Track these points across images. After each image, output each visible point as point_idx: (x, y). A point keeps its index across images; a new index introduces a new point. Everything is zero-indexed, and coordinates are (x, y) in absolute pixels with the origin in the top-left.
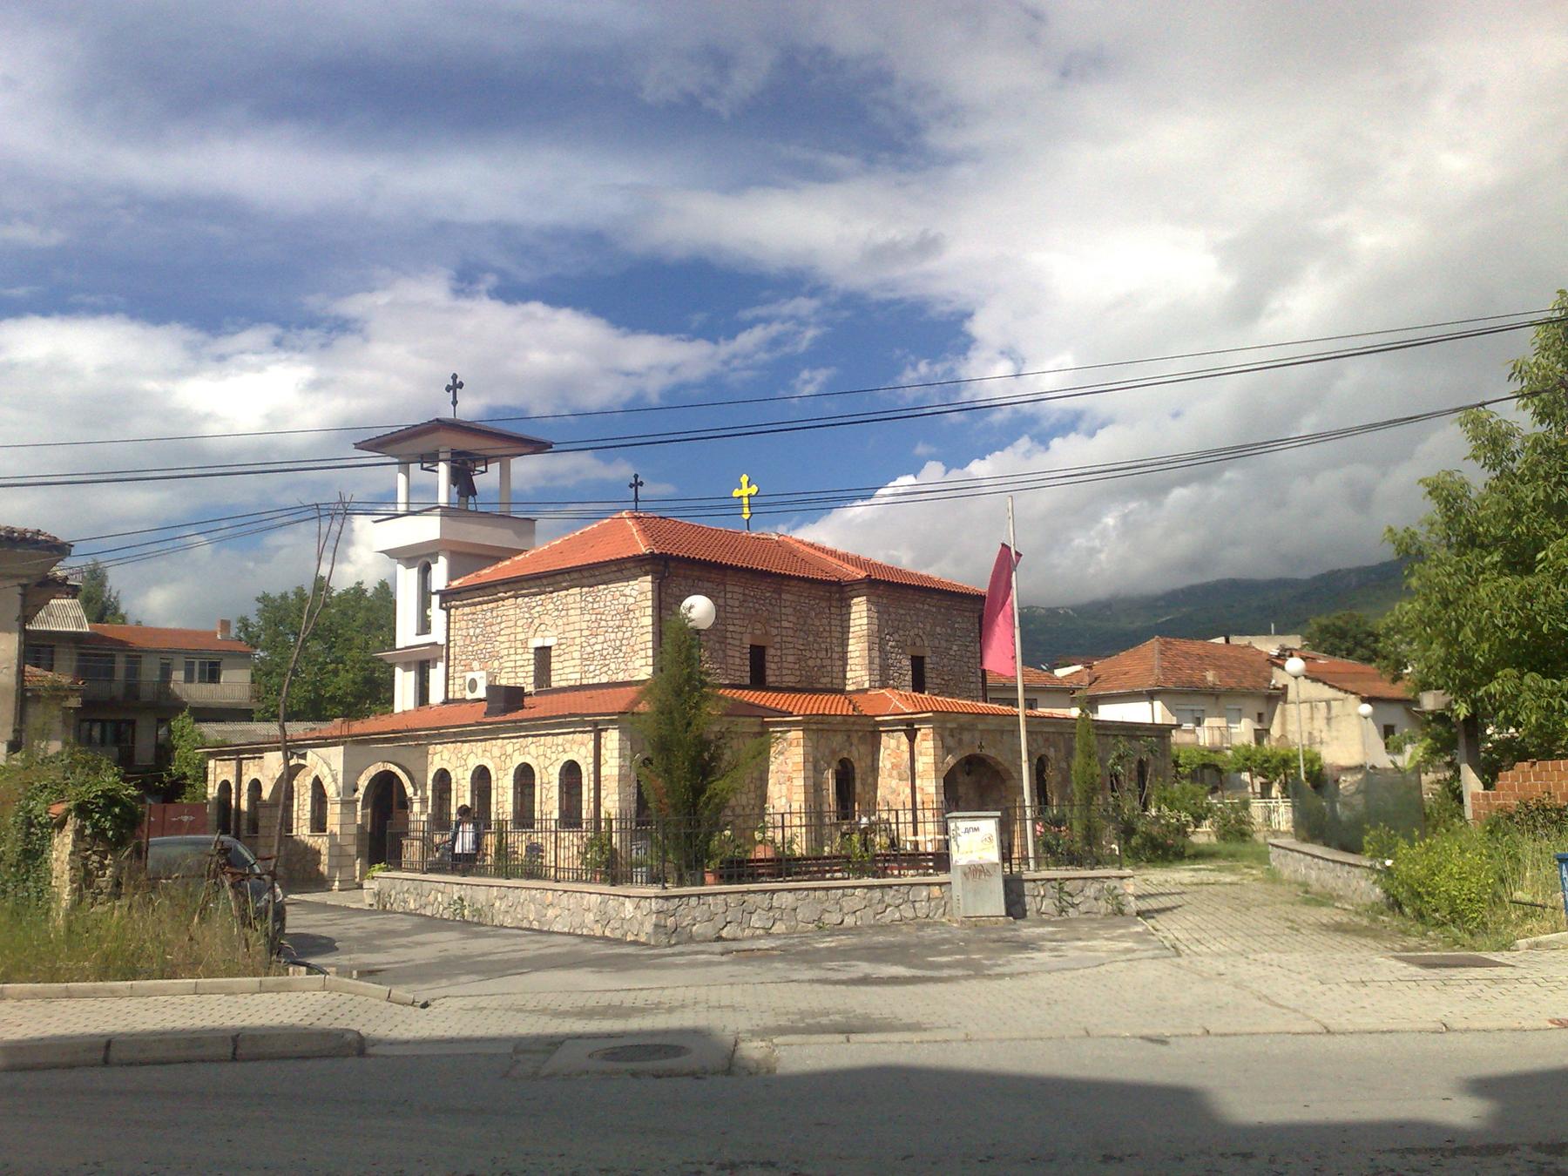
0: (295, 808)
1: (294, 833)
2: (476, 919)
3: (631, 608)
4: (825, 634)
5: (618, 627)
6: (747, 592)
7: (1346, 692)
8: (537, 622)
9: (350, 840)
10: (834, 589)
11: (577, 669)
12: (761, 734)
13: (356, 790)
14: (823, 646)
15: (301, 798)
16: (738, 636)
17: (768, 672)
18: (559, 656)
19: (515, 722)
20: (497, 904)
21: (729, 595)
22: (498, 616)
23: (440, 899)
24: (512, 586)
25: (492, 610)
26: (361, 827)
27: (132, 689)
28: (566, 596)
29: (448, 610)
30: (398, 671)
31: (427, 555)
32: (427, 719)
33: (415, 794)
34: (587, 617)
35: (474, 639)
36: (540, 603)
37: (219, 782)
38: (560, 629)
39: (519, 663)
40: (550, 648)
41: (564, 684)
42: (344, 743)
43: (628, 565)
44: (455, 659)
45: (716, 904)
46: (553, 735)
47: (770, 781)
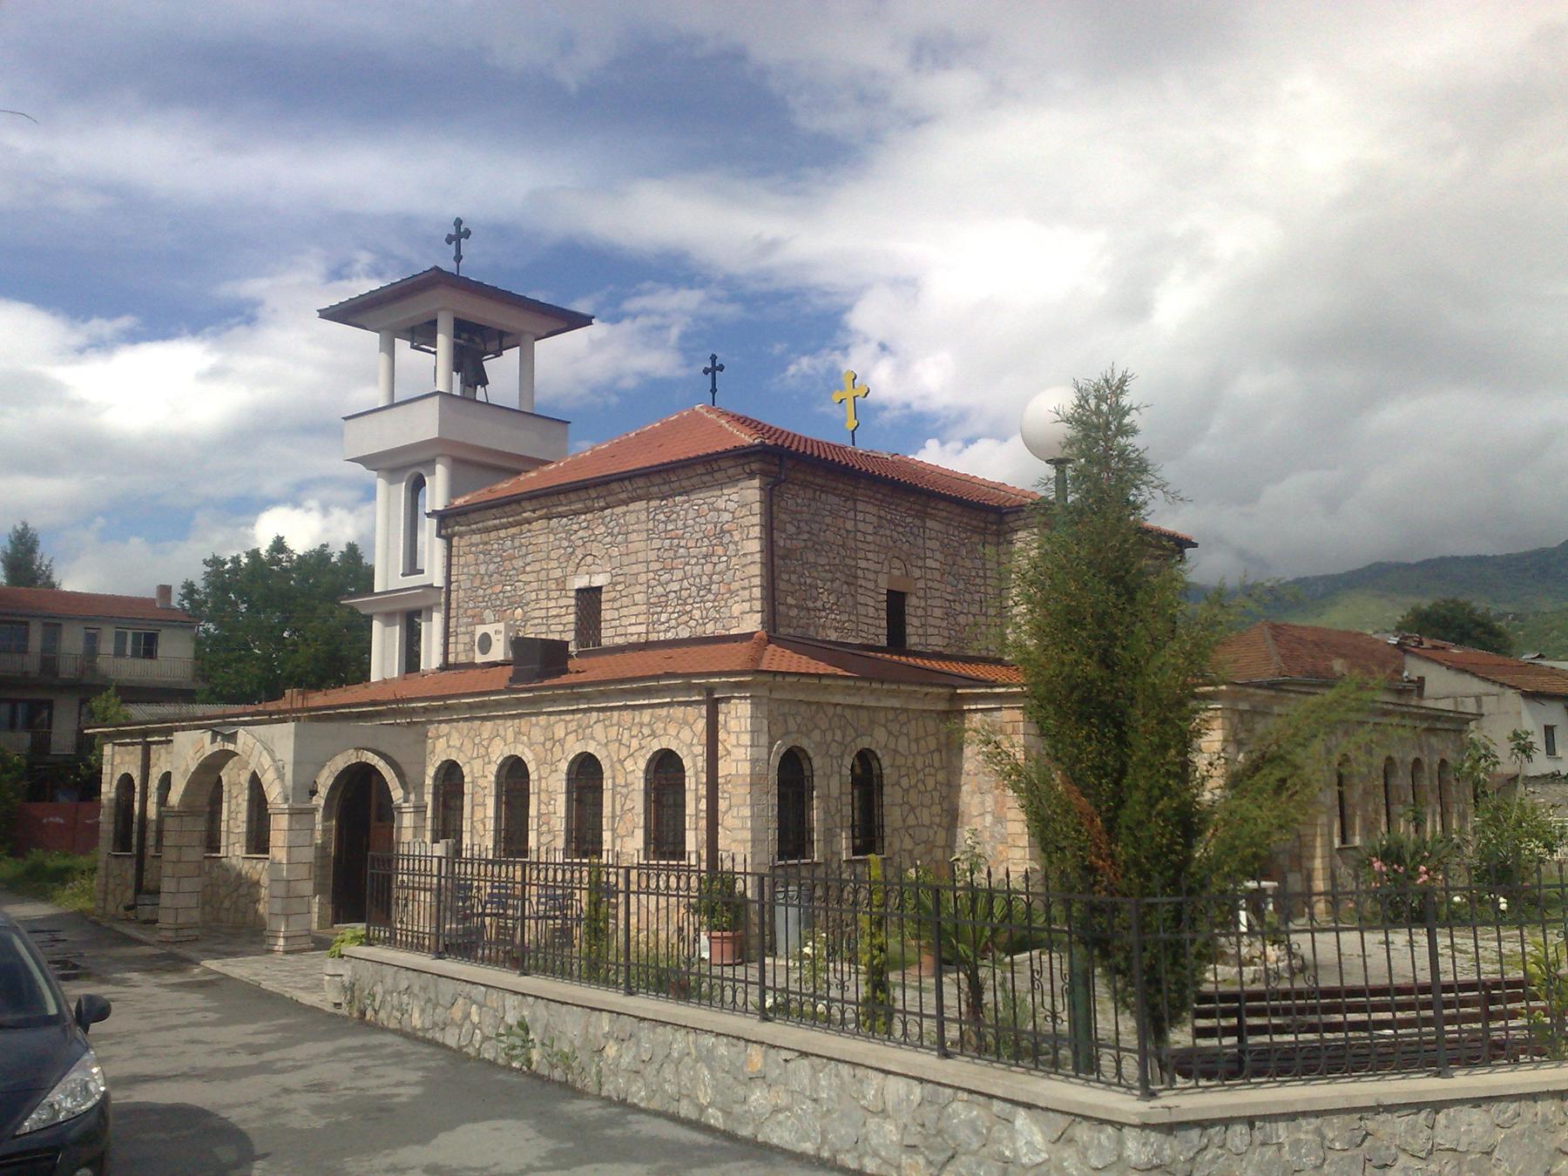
0: (224, 816)
1: (223, 853)
2: (557, 1074)
3: (726, 527)
4: (978, 580)
5: (705, 557)
6: (882, 513)
7: (1502, 685)
8: (579, 553)
9: (303, 871)
10: (992, 517)
11: (641, 619)
12: (946, 715)
13: (313, 792)
14: (977, 597)
15: (234, 801)
16: (871, 576)
17: (909, 630)
18: (614, 600)
19: (572, 686)
20: (611, 1050)
21: (860, 516)
22: (522, 545)
23: (475, 1019)
24: (542, 500)
25: (513, 537)
26: (323, 848)
27: (49, 664)
28: (624, 514)
29: (448, 539)
30: (377, 626)
31: (418, 464)
32: (414, 687)
33: (406, 801)
34: (657, 544)
35: (486, 579)
36: (584, 525)
37: (117, 776)
38: (616, 562)
39: (553, 612)
40: (599, 589)
41: (620, 641)
42: (297, 719)
43: (723, 464)
44: (458, 607)
45: (1296, 1144)
46: (634, 707)
47: (964, 788)
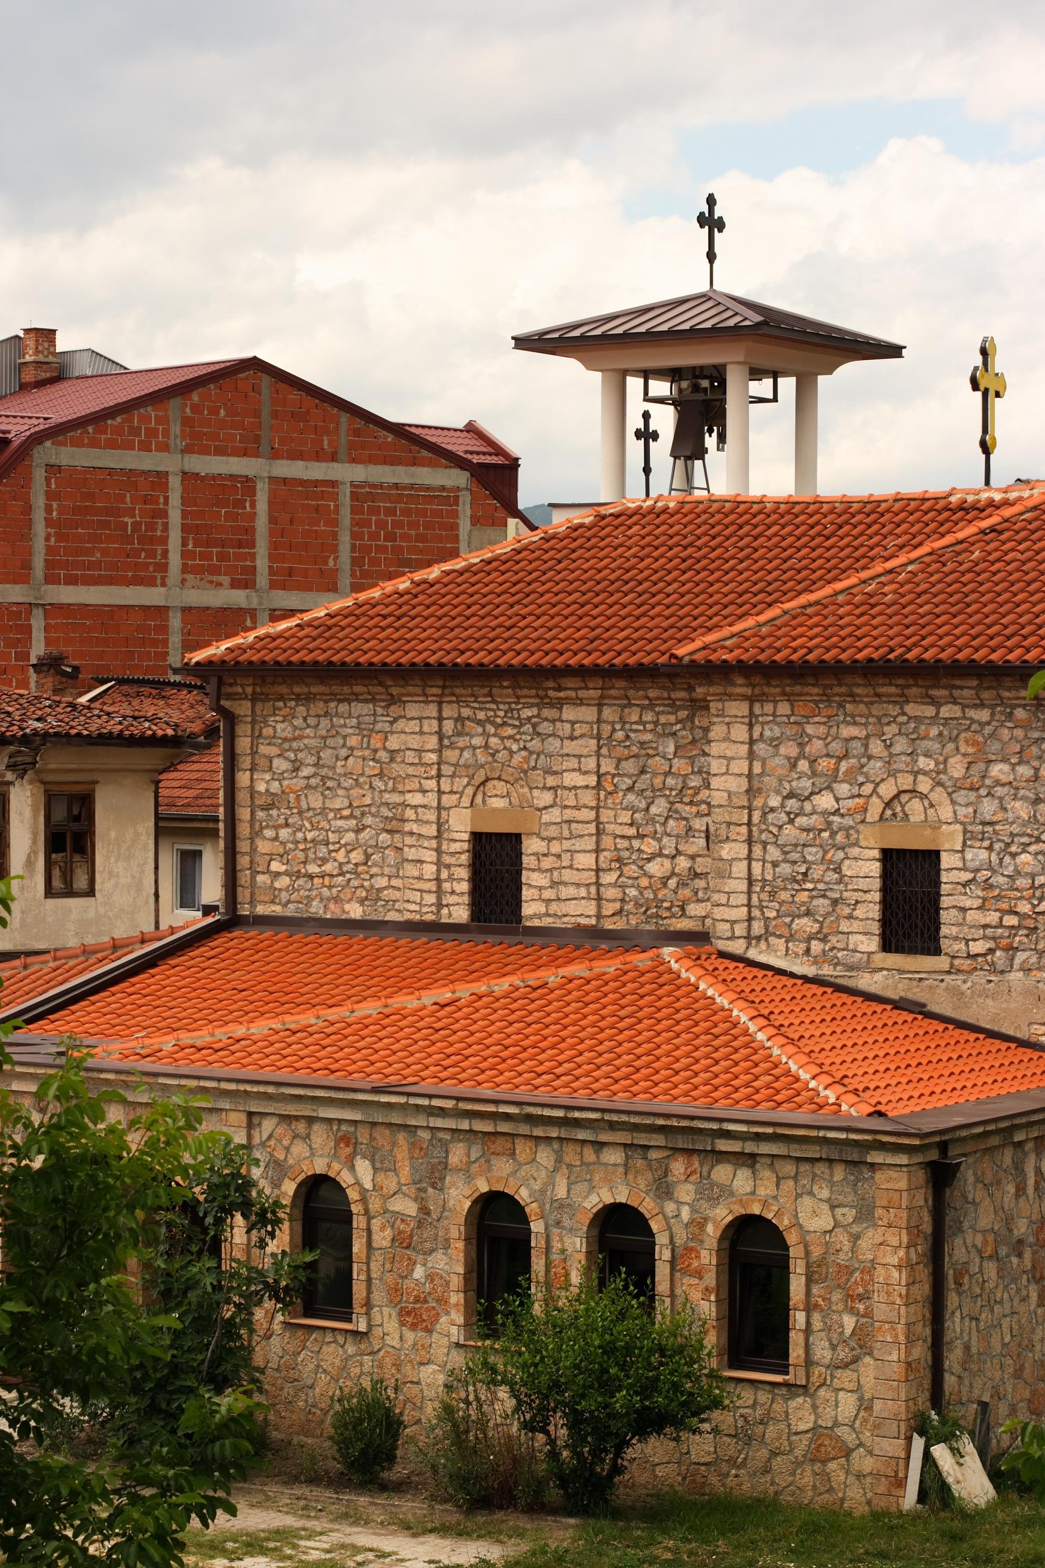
17: (526, 893)
